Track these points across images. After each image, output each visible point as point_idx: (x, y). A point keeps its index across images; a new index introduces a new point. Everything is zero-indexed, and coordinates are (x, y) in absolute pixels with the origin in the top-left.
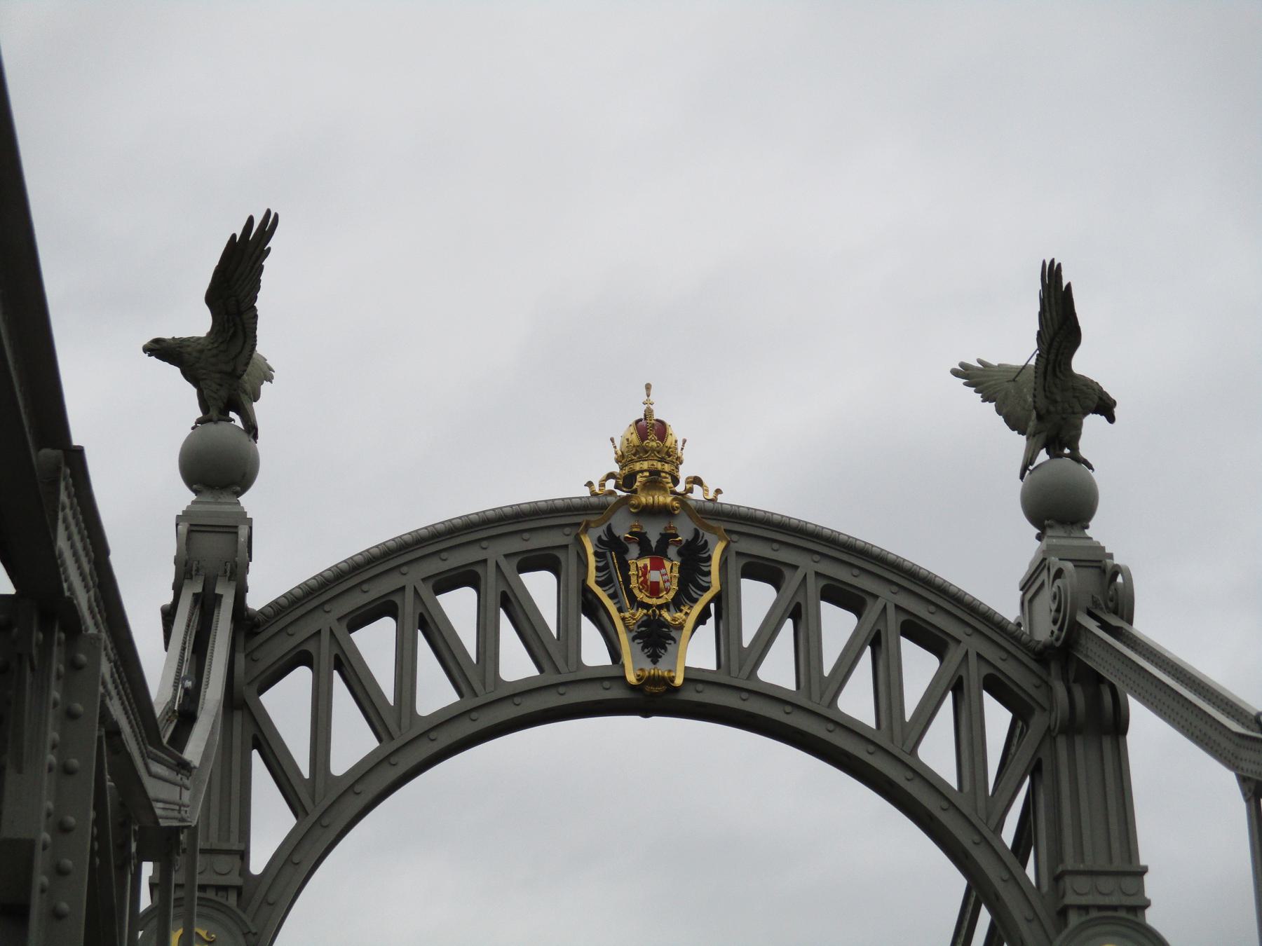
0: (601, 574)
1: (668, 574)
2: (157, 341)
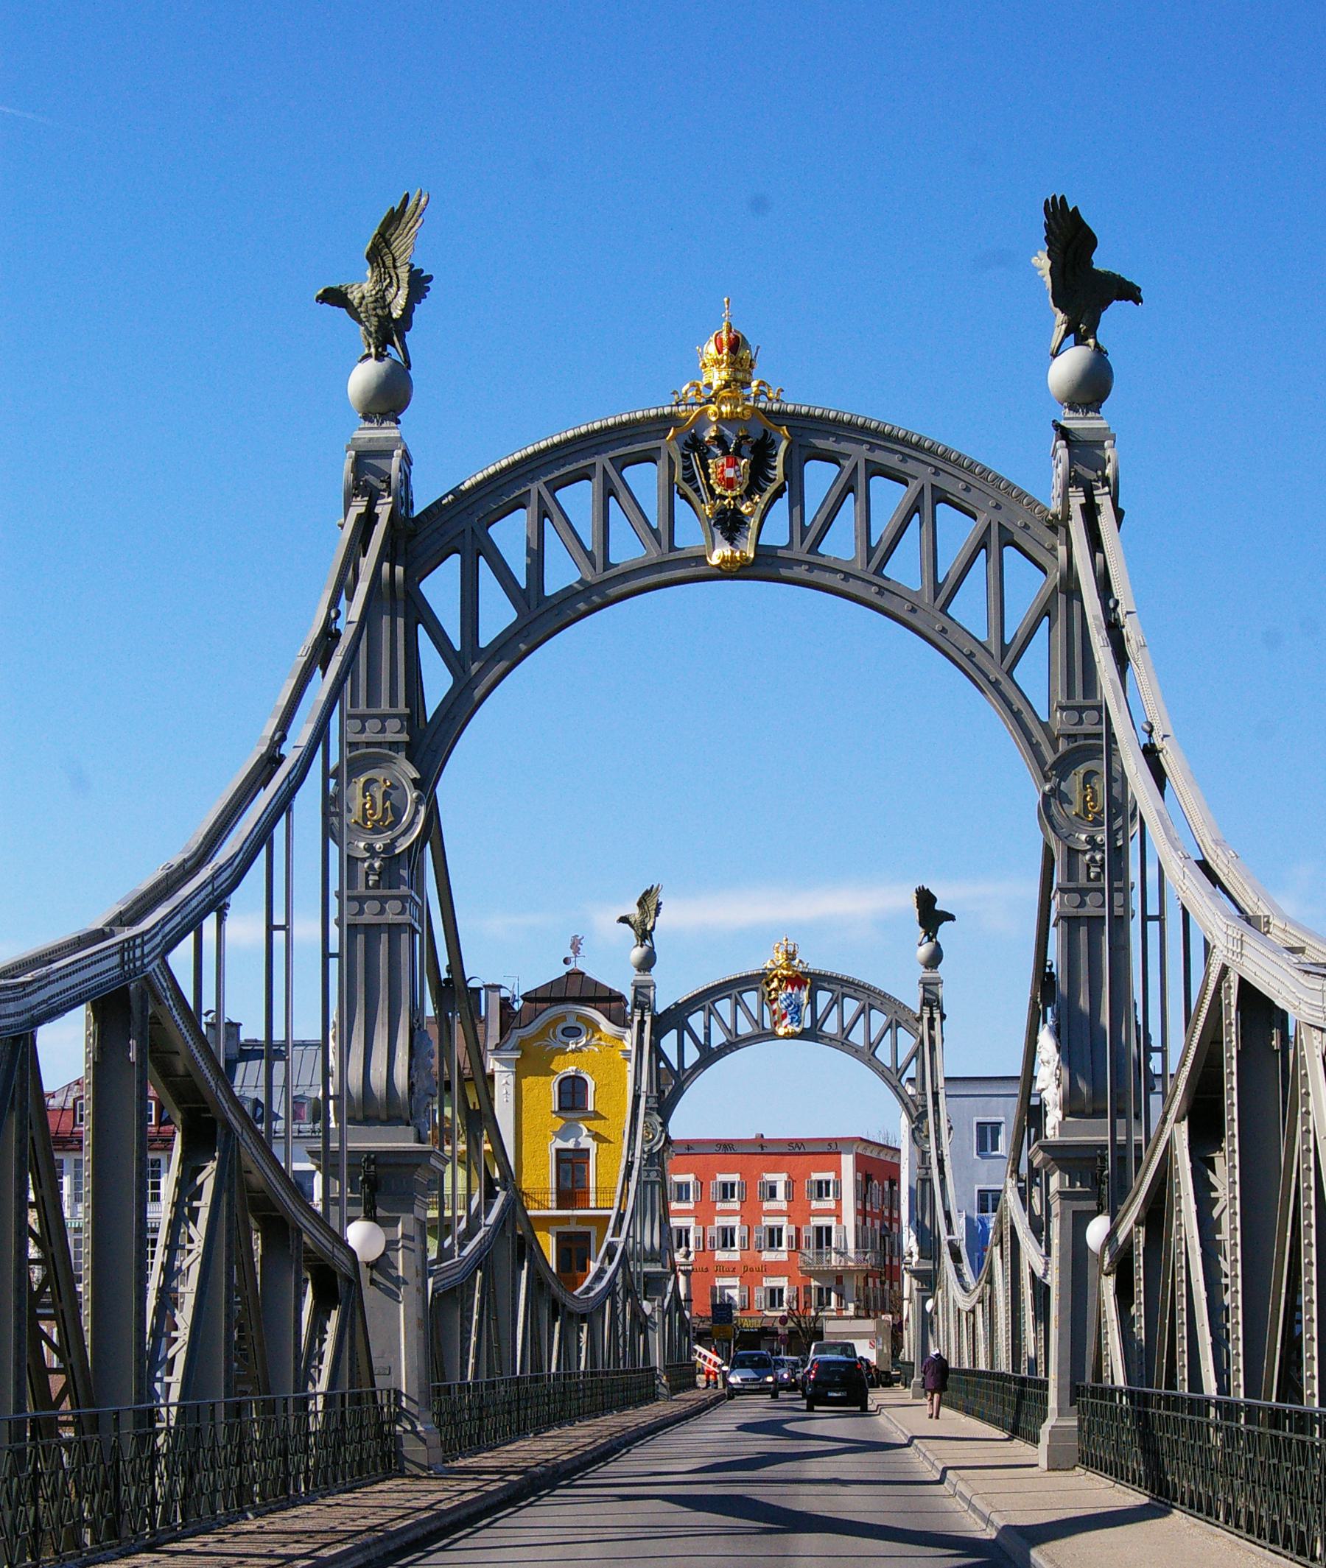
0: (685, 472)
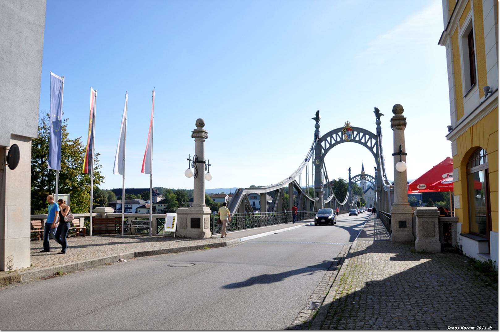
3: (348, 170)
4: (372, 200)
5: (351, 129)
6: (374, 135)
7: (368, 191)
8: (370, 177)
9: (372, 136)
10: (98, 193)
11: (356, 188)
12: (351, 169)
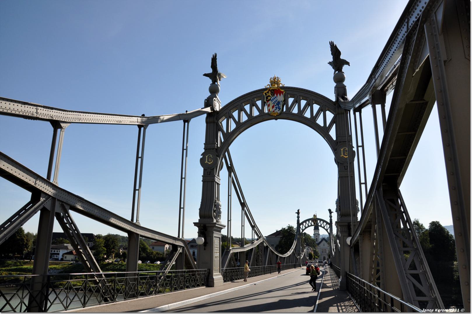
1: (315, 221)
2: (205, 74)
3: (296, 213)
4: (326, 252)
5: (282, 91)
6: (331, 101)
7: (322, 242)
8: (323, 222)
9: (327, 223)
10: (21, 236)
11: (309, 239)
12: (300, 211)
